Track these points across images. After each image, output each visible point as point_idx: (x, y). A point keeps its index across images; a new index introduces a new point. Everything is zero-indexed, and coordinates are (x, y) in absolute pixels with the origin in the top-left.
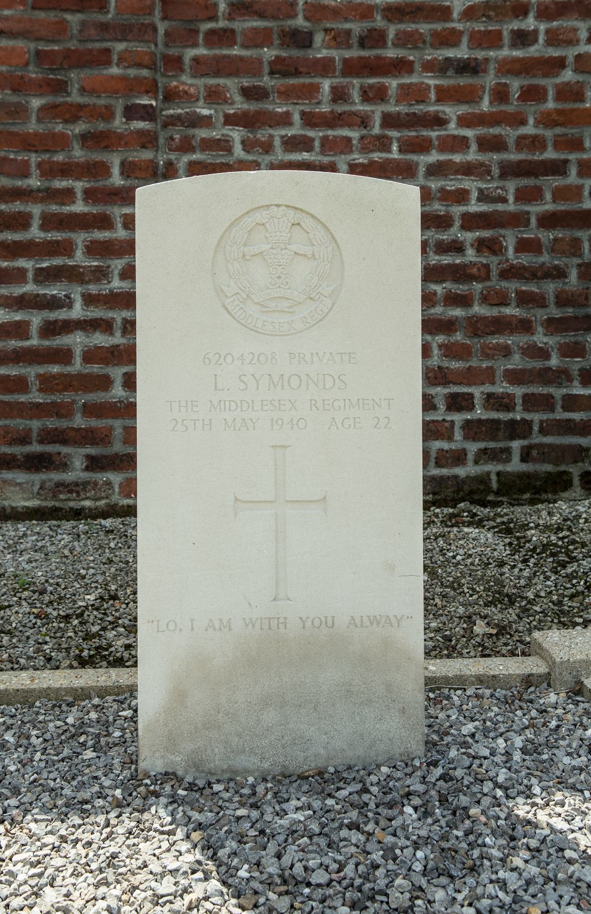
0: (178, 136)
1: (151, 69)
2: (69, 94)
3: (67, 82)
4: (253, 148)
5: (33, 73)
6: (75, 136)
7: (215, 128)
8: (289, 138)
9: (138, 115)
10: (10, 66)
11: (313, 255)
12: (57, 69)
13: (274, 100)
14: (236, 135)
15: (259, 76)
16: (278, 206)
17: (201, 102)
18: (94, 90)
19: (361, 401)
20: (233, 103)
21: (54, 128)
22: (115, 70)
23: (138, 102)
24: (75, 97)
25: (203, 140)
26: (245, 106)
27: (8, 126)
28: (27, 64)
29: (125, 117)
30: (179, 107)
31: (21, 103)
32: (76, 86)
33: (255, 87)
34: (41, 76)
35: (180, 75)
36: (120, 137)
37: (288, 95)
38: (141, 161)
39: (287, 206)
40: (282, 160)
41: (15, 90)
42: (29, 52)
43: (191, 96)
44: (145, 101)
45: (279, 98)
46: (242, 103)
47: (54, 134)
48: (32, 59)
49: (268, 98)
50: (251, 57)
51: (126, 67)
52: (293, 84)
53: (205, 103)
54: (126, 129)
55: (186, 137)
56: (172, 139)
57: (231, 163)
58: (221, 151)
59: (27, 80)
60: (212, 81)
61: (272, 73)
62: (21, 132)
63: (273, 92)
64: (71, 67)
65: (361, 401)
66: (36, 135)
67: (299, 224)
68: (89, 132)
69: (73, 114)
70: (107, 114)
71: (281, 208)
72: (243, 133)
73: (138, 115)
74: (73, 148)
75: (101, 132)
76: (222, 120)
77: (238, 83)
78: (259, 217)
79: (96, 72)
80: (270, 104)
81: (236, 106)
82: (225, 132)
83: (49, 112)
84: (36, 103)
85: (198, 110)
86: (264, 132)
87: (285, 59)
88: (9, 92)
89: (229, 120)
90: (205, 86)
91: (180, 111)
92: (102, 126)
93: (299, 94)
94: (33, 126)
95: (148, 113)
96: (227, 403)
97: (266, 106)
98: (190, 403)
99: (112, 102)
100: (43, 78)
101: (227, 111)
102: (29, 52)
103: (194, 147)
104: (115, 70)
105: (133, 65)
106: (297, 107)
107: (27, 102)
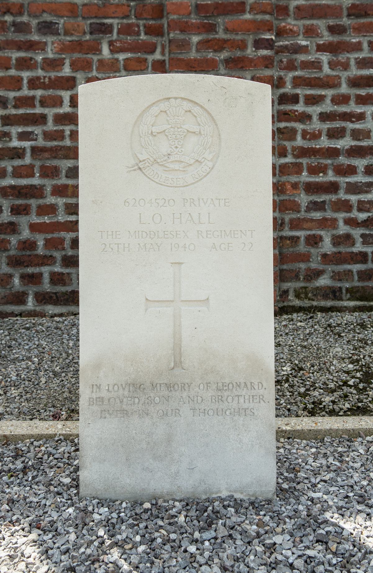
0: (285, 60)
1: (272, 15)
2: (217, 33)
3: (216, 25)
4: (336, 67)
5: (194, 20)
6: (221, 60)
7: (310, 54)
8: (361, 59)
9: (263, 46)
10: (179, 15)
11: (200, 132)
12: (210, 16)
13: (350, 34)
14: (325, 58)
15: (340, 18)
16: (176, 98)
17: (301, 37)
18: (234, 29)
19: (232, 232)
20: (322, 37)
21: (207, 56)
22: (248, 16)
23: (263, 37)
24: (221, 35)
25: (302, 62)
26: (331, 39)
27: (177, 55)
28: (190, 14)
29: (254, 47)
30: (286, 40)
31: (186, 39)
32: (222, 27)
33: (337, 25)
34: (199, 21)
35: (287, 19)
36: (251, 61)
37: (360, 30)
38: (265, 76)
39: (182, 98)
40: (355, 75)
41: (182, 31)
42: (191, 5)
43: (295, 32)
44: (267, 36)
45: (353, 32)
46: (329, 36)
47: (207, 60)
48: (193, 11)
49: (346, 33)
50: (335, 5)
51: (255, 14)
52: (363, 23)
53: (304, 37)
54: (255, 56)
55: (290, 60)
56: (281, 61)
57: (322, 77)
58: (315, 69)
59: (190, 24)
60: (308, 22)
61: (349, 15)
62: (186, 59)
63: (350, 29)
64: (219, 15)
65: (232, 232)
66: (195, 60)
67: (165, 112)
68: (231, 58)
69: (220, 45)
70: (243, 46)
71: (178, 100)
72: (329, 57)
73: (263, 46)
74: (219, 69)
75: (239, 57)
76: (315, 48)
77: (326, 23)
78: (163, 106)
79: (235, 18)
80: (348, 36)
81: (324, 39)
82: (317, 56)
83: (204, 45)
84: (195, 39)
85: (299, 42)
86: (343, 56)
87: (358, 5)
88: (178, 32)
89: (320, 48)
90: (304, 25)
91: (287, 43)
92: (239, 54)
93: (368, 29)
94: (193, 55)
95: (269, 44)
96: (140, 233)
97: (345, 38)
98: (114, 233)
99: (245, 37)
100: (200, 22)
101: (318, 42)
102: (191, 5)
103: (296, 67)
104: (248, 16)
105: (260, 13)
106: (366, 38)
107: (190, 39)
